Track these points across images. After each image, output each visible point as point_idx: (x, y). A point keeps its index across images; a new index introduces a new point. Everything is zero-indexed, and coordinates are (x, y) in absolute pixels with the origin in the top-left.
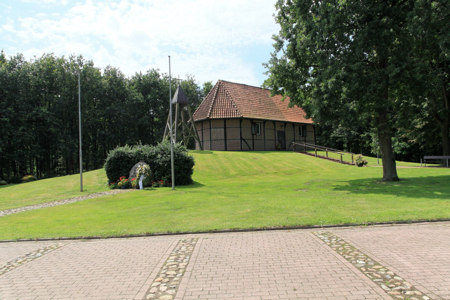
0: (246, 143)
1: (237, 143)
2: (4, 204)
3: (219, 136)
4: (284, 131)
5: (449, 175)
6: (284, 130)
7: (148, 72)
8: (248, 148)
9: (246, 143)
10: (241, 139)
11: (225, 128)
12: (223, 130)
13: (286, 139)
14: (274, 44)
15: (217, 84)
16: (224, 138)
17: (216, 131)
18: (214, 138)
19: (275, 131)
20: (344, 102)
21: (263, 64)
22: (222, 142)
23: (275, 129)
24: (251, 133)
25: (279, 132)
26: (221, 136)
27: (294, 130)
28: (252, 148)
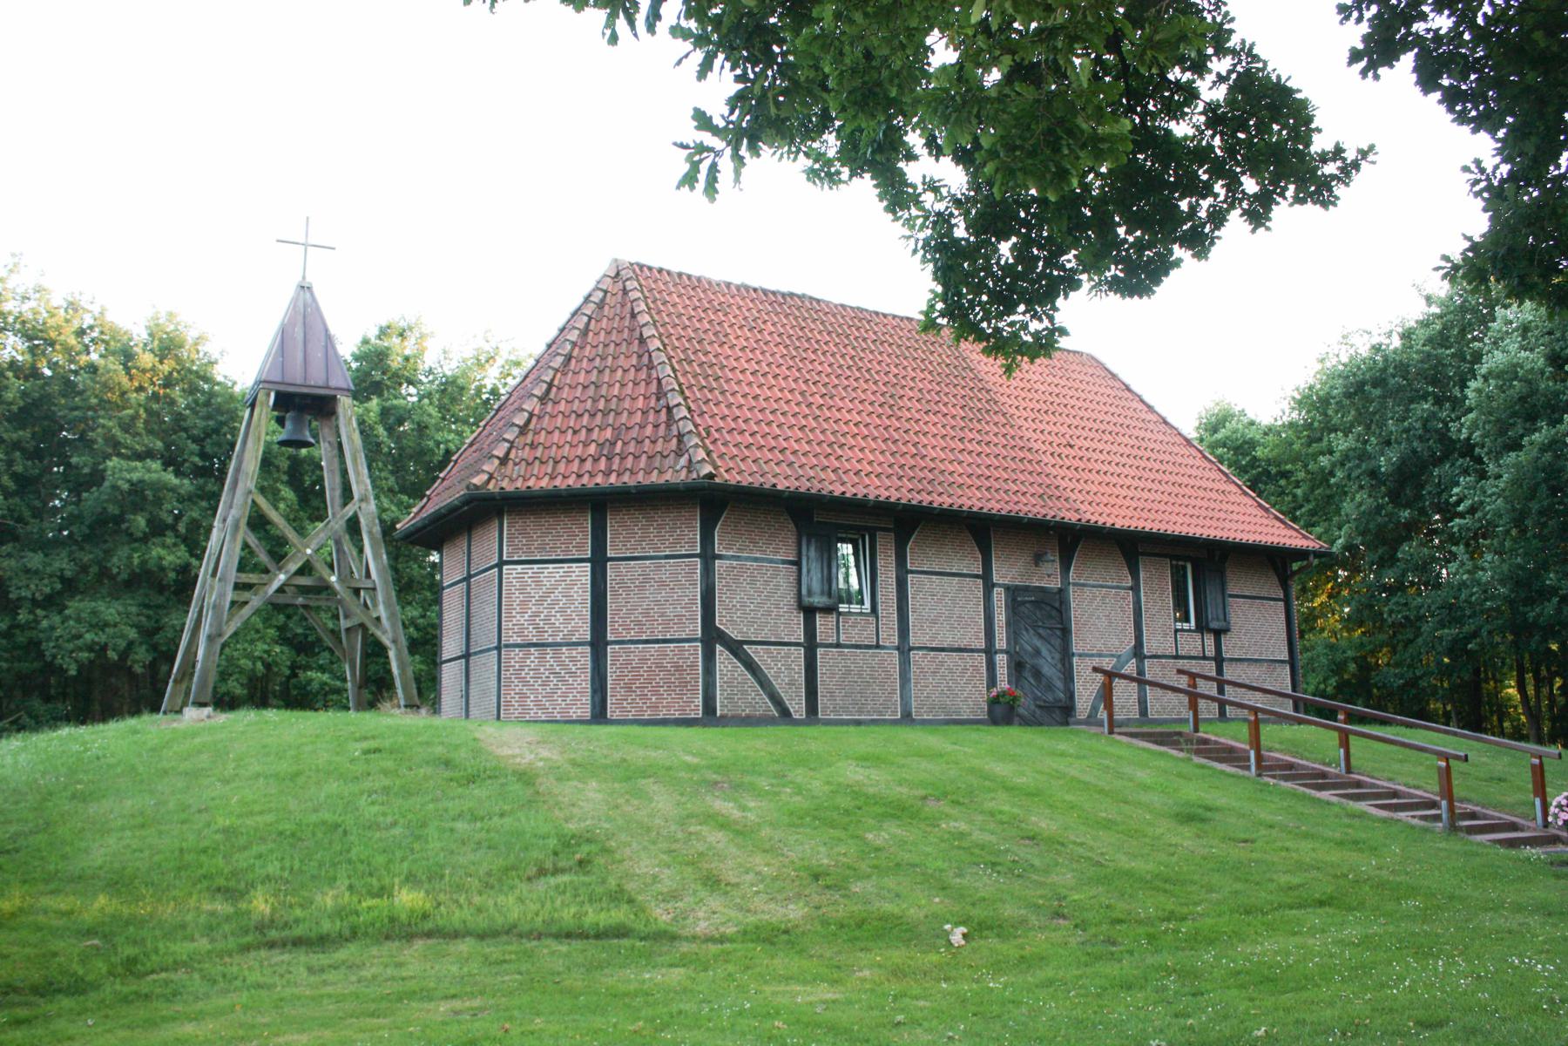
1: (678, 668)
3: (558, 620)
4: (1062, 592)
5: (15, 742)
8: (766, 706)
10: (712, 636)
11: (599, 562)
12: (583, 573)
15: (587, 299)
16: (585, 632)
17: (538, 583)
18: (520, 634)
19: (989, 587)
22: (574, 660)
23: (986, 577)
24: (790, 599)
25: (1014, 594)
26: (568, 620)
28: (797, 707)
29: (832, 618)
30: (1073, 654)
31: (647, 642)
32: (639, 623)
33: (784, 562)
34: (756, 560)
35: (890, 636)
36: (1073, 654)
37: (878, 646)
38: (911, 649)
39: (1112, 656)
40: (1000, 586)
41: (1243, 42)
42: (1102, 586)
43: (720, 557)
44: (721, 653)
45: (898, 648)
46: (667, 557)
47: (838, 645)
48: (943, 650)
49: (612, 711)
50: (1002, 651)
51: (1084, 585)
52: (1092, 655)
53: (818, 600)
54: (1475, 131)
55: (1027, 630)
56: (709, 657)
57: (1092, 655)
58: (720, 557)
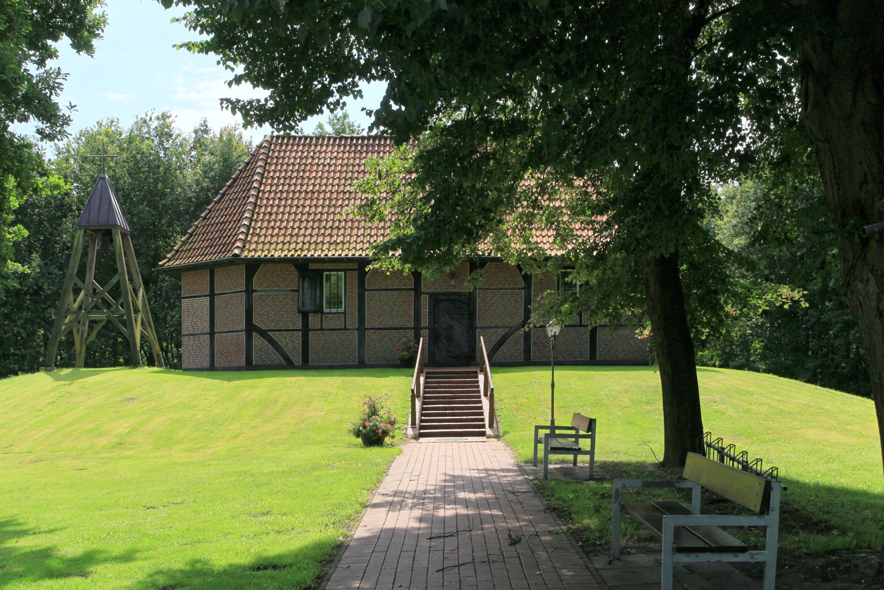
0: (272, 341)
2: (59, 469)
3: (199, 324)
8: (278, 359)
9: (272, 341)
10: (250, 328)
11: (212, 295)
13: (479, 323)
16: (207, 330)
18: (187, 330)
20: (86, 159)
28: (297, 359)
29: (319, 316)
30: (476, 328)
31: (227, 332)
32: (224, 324)
33: (291, 291)
34: (276, 291)
35: (353, 322)
36: (476, 328)
37: (345, 329)
38: (366, 329)
39: (506, 327)
40: (426, 293)
41: (51, 68)
42: (501, 289)
43: (256, 291)
44: (256, 337)
45: (358, 329)
46: (235, 292)
47: (322, 329)
48: (386, 329)
49: (217, 365)
50: (425, 328)
51: (488, 289)
52: (491, 328)
53: (308, 307)
54: (207, 53)
55: (443, 315)
56: (249, 339)
57: (491, 328)
58: (256, 291)
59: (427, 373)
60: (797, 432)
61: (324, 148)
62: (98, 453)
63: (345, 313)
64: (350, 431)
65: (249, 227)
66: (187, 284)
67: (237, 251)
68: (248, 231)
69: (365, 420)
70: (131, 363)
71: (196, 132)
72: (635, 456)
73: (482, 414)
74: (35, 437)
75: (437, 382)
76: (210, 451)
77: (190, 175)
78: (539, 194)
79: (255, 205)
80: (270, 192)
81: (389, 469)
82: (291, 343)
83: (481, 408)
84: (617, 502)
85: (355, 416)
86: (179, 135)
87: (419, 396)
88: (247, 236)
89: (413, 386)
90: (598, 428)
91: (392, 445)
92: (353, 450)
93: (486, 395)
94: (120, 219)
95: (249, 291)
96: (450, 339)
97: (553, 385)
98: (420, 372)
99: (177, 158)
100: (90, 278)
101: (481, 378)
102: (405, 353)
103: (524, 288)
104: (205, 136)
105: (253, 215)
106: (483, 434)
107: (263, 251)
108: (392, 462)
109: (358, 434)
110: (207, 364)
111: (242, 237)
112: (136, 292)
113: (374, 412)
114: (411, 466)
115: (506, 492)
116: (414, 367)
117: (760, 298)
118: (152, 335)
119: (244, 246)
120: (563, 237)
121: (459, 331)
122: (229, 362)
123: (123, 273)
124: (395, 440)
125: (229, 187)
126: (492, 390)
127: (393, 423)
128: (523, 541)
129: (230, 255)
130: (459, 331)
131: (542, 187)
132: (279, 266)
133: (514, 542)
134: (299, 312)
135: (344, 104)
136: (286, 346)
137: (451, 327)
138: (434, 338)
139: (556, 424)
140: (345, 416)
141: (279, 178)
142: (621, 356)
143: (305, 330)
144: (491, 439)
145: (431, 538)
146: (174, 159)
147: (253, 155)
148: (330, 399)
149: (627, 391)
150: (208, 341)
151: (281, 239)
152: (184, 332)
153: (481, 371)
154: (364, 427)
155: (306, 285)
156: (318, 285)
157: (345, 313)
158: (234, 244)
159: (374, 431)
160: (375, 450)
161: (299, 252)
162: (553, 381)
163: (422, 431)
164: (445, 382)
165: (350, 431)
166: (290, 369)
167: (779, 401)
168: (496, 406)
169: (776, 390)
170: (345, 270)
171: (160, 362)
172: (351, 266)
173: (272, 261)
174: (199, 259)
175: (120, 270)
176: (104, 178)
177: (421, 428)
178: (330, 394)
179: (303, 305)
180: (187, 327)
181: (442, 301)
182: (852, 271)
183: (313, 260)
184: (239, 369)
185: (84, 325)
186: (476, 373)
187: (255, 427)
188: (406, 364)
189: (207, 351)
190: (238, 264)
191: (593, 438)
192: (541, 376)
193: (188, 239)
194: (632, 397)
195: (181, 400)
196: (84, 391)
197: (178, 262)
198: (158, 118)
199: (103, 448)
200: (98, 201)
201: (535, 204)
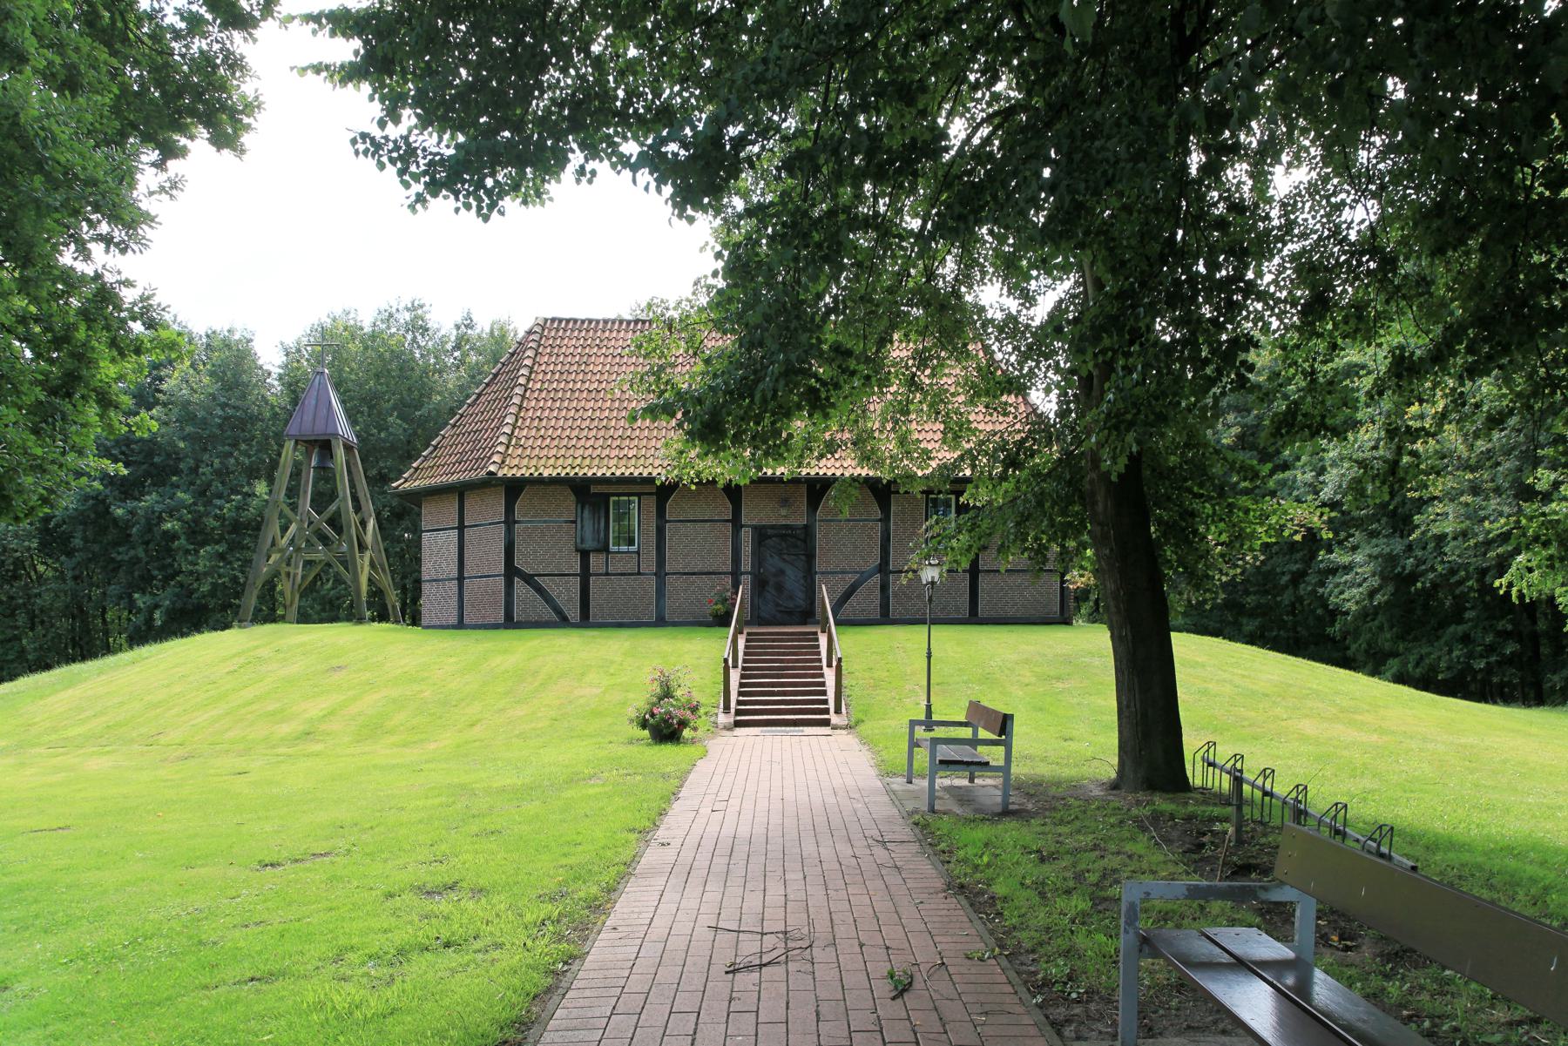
0: (539, 590)
6: (803, 521)
7: (691, 220)
8: (555, 618)
9: (539, 590)
10: (511, 571)
11: (461, 528)
13: (819, 565)
14: (199, 146)
16: (455, 574)
21: (412, 207)
27: (886, 519)
28: (574, 613)
29: (603, 556)
33: (566, 522)
34: (545, 522)
35: (649, 564)
37: (639, 573)
47: (607, 574)
48: (694, 574)
49: (466, 621)
59: (749, 634)
60: (1283, 723)
61: (614, 334)
62: (274, 747)
63: (638, 553)
64: (631, 721)
65: (511, 436)
66: (430, 514)
67: (492, 468)
68: (510, 442)
69: (654, 705)
70: (354, 617)
71: (458, 327)
72: (1058, 764)
73: (824, 693)
74: (195, 722)
75: (761, 647)
76: (432, 746)
77: (451, 380)
78: (918, 369)
79: (520, 407)
80: (541, 391)
81: (682, 786)
82: (566, 593)
83: (823, 684)
84: (1131, 931)
85: (640, 699)
86: (438, 330)
87: (735, 666)
88: (508, 448)
89: (726, 652)
90: (1018, 728)
91: (693, 741)
92: (634, 749)
93: (829, 665)
94: (343, 427)
95: (510, 522)
96: (780, 588)
97: (929, 656)
98: (738, 631)
99: (436, 357)
100: (304, 505)
101: (823, 641)
102: (719, 606)
103: (880, 520)
104: (469, 332)
105: (517, 421)
106: (826, 723)
107: (528, 468)
108: (689, 772)
109: (644, 724)
110: (454, 620)
111: (501, 449)
112: (363, 523)
113: (667, 693)
114: (717, 779)
115: (870, 841)
116: (728, 625)
117: (1262, 524)
118: (386, 581)
119: (503, 462)
120: (955, 432)
121: (793, 578)
122: (484, 617)
123: (345, 498)
124: (700, 733)
125: (488, 385)
126: (840, 660)
127: (694, 709)
128: (918, 984)
129: (483, 473)
130: (793, 578)
131: (922, 359)
132: (551, 488)
133: (902, 989)
134: (577, 550)
135: (593, 173)
136: (559, 597)
137: (782, 572)
138: (760, 585)
139: (935, 718)
140: (631, 695)
141: (553, 373)
142: (1011, 613)
143: (585, 575)
144: (838, 731)
145: (733, 972)
146: (432, 361)
147: (520, 343)
148: (612, 671)
149: (1027, 661)
150: (456, 589)
151: (554, 452)
152: (425, 577)
153: (823, 632)
154: (653, 715)
155: (586, 513)
156: (602, 514)
157: (638, 553)
158: (490, 458)
159: (666, 721)
160: (668, 750)
161: (577, 470)
162: (929, 649)
163: (739, 718)
164: (772, 647)
165: (631, 721)
166: (564, 627)
167: (1244, 676)
168: (845, 682)
169: (1234, 660)
170: (639, 495)
171: (396, 616)
172: (647, 489)
173: (540, 481)
174: (444, 479)
175: (341, 494)
176: (322, 373)
177: (738, 712)
178: (612, 662)
179: (582, 541)
180: (428, 570)
181: (770, 537)
182: (367, 688)
183: (595, 480)
184: (495, 627)
185: (296, 567)
186: (816, 633)
187: (503, 710)
188: (722, 620)
189: (454, 602)
190: (495, 486)
191: (1008, 745)
192: (909, 639)
193: (431, 453)
194: (1036, 669)
195: (406, 669)
196: (282, 655)
197: (416, 483)
198: (408, 309)
199: (282, 739)
200: (314, 402)
201: (912, 383)
